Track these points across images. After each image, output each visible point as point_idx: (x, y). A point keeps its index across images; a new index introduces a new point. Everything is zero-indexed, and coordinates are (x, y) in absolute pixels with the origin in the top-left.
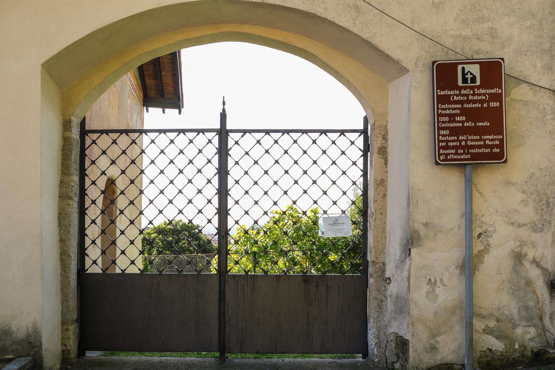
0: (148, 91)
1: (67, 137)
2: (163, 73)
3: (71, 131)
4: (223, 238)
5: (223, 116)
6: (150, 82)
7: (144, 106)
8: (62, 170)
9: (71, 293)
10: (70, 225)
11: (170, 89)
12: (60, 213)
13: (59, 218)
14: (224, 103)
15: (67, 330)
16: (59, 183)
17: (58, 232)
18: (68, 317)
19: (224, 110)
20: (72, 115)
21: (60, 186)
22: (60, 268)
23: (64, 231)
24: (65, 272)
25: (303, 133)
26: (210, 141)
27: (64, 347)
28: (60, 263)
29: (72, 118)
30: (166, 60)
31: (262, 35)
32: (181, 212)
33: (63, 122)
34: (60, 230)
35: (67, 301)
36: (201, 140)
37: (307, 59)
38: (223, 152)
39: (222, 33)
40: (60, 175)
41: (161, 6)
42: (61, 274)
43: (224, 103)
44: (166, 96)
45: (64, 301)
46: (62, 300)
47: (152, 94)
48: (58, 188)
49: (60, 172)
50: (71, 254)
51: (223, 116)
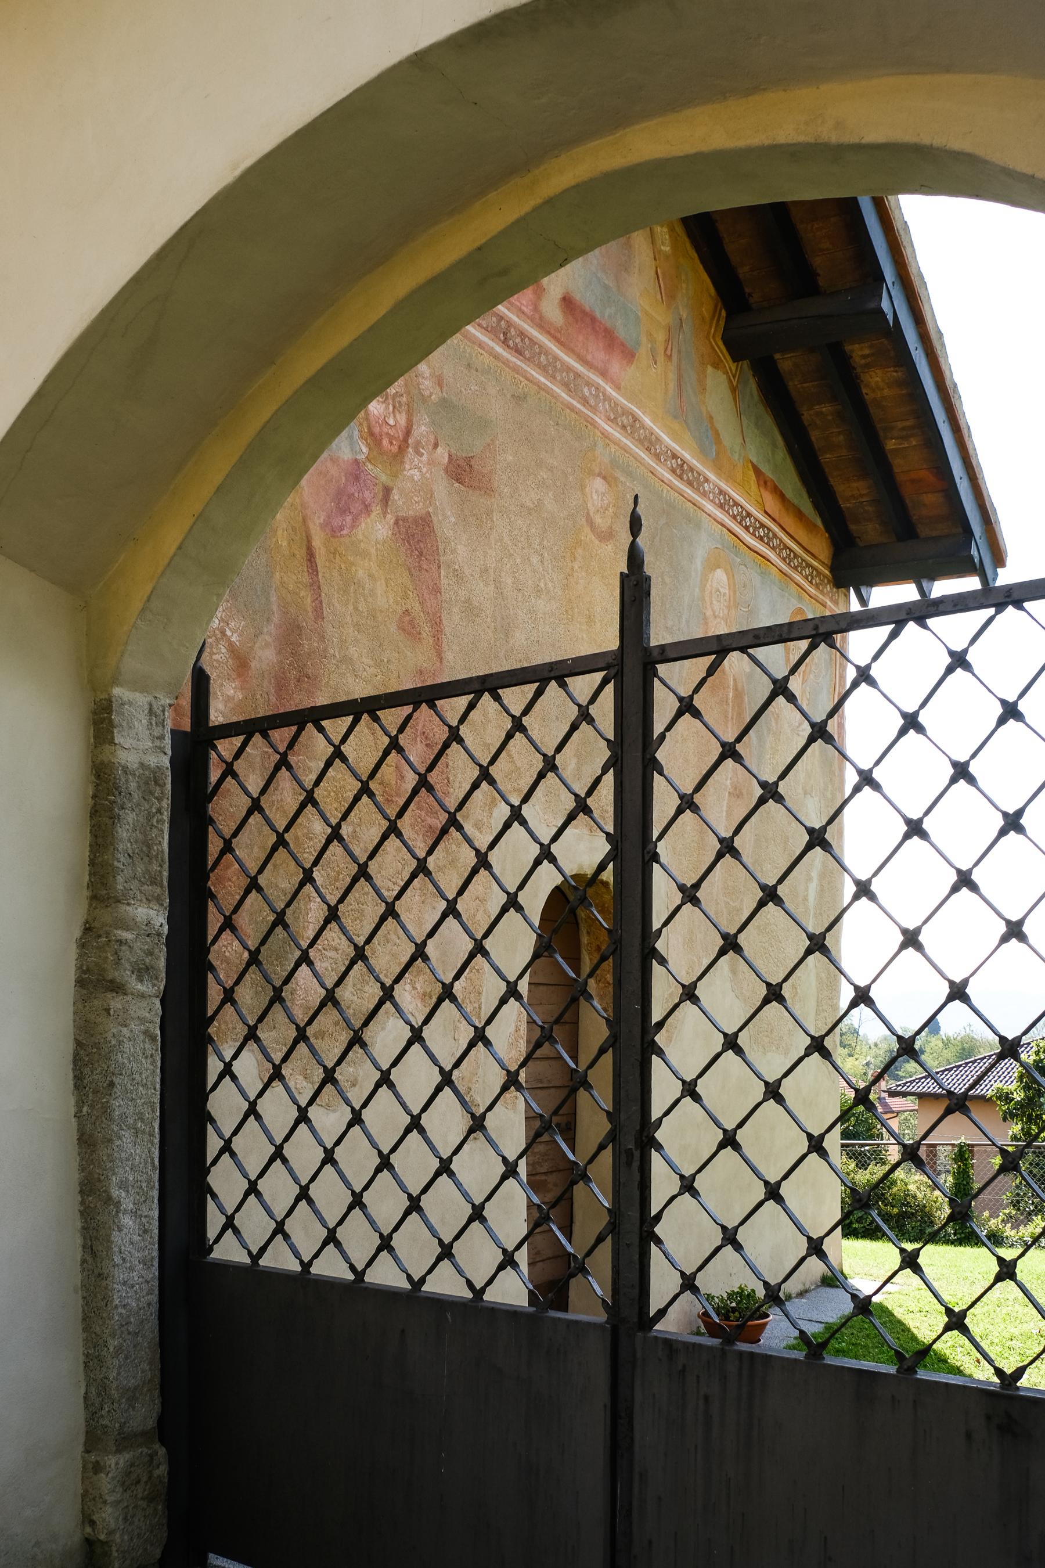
0: (853, 527)
1: (102, 763)
2: (891, 445)
3: (112, 742)
4: (629, 1164)
5: (635, 591)
6: (853, 491)
7: (847, 587)
8: (90, 885)
9: (113, 1335)
10: (112, 1084)
11: (927, 504)
12: (78, 1044)
13: (77, 1059)
14: (635, 525)
15: (97, 1468)
16: (77, 933)
17: (73, 1110)
18: (106, 1422)
19: (635, 558)
20: (115, 681)
21: (82, 945)
22: (79, 1241)
23: (92, 1107)
24: (94, 1254)
25: (1000, 607)
26: (585, 716)
27: (88, 1530)
28: (79, 1224)
29: (117, 691)
30: (886, 392)
31: (705, 148)
32: (958, 992)
33: (95, 713)
34: (80, 1104)
35: (100, 1359)
36: (553, 712)
37: (977, 196)
38: (634, 756)
39: (549, 202)
40: (85, 904)
41: (238, 172)
42: (84, 1261)
43: (635, 525)
44: (924, 531)
45: (92, 1360)
46: (87, 1355)
47: (869, 531)
48: (73, 952)
49: (86, 893)
50: (115, 1192)
51: (635, 591)
